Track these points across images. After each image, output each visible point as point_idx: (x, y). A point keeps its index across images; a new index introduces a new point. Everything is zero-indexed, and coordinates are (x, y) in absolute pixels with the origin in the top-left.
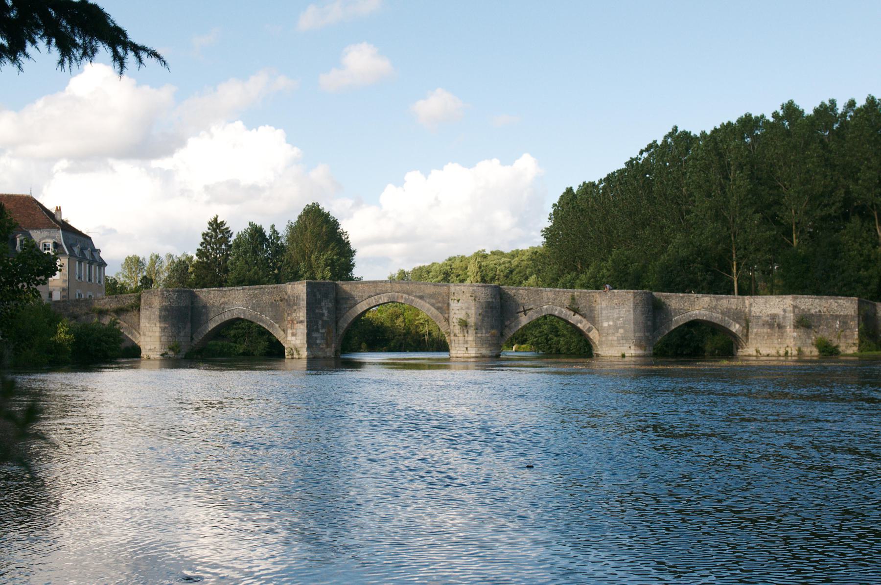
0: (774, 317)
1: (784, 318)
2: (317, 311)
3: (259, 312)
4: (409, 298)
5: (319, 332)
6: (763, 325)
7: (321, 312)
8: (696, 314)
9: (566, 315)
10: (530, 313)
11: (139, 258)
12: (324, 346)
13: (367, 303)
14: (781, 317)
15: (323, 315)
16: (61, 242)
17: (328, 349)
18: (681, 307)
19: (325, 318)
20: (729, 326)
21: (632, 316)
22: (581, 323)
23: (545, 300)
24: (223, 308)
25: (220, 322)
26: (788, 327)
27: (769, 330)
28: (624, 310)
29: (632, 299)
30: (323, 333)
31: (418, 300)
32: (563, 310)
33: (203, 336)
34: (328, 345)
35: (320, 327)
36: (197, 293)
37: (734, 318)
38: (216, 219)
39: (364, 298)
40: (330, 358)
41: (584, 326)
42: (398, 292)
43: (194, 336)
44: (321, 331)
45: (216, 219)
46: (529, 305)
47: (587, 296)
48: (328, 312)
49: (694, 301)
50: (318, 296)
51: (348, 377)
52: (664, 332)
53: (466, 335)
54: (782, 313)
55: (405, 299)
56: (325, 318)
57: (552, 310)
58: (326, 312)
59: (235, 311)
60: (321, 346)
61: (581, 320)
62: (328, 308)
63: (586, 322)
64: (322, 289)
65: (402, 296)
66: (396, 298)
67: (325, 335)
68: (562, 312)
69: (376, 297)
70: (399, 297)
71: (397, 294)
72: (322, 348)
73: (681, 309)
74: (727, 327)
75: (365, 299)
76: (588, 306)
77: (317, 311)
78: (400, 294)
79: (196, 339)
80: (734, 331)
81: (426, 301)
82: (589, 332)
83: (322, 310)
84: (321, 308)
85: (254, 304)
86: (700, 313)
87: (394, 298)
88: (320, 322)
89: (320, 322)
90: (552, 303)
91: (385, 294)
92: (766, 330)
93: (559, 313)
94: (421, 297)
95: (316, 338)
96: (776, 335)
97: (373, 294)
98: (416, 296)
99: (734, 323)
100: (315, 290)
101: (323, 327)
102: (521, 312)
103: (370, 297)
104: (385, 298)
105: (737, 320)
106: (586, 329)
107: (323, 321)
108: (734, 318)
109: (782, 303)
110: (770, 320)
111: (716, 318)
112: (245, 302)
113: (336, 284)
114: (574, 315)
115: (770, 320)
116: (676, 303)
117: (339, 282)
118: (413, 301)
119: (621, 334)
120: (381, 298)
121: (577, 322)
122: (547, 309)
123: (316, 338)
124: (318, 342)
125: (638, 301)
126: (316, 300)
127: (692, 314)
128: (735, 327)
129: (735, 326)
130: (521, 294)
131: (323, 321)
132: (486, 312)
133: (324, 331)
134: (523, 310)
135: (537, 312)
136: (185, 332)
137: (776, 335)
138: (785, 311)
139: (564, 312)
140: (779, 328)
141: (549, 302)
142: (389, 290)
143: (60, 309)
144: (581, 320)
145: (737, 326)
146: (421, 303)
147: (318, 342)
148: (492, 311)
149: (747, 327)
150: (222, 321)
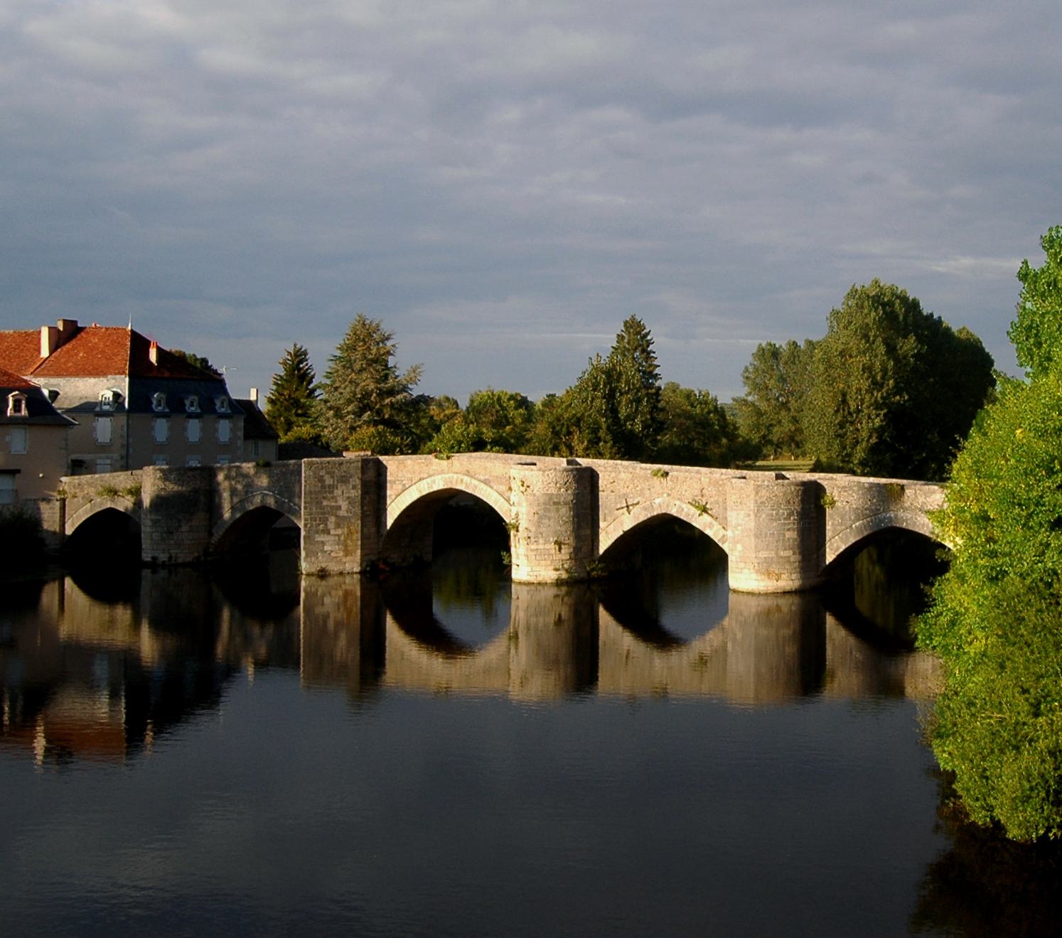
2: (325, 503)
3: (287, 498)
4: (471, 483)
5: (329, 533)
7: (333, 504)
10: (634, 510)
12: (341, 554)
13: (417, 489)
15: (339, 508)
16: (125, 393)
17: (349, 558)
19: (342, 513)
21: (753, 524)
29: (752, 496)
31: (483, 485)
32: (684, 506)
33: (224, 530)
34: (347, 553)
35: (331, 525)
36: (384, 462)
39: (414, 482)
43: (214, 531)
46: (633, 497)
47: (721, 485)
50: (328, 481)
51: (831, 657)
55: (466, 484)
56: (342, 513)
58: (344, 505)
60: (333, 554)
61: (711, 523)
65: (462, 480)
67: (342, 538)
69: (429, 480)
71: (455, 476)
72: (336, 557)
75: (415, 483)
76: (721, 500)
77: (325, 503)
78: (460, 476)
81: (492, 488)
83: (336, 502)
85: (281, 486)
87: (451, 482)
88: (332, 519)
89: (332, 519)
91: (440, 476)
94: (486, 482)
95: (323, 543)
98: (480, 481)
100: (322, 473)
101: (338, 526)
102: (623, 508)
111: (923, 525)
113: (379, 463)
117: (381, 458)
118: (476, 487)
120: (434, 482)
123: (323, 543)
125: (764, 500)
126: (323, 487)
131: (337, 517)
132: (546, 510)
133: (339, 531)
134: (625, 505)
136: (191, 526)
139: (686, 510)
142: (446, 471)
144: (711, 523)
146: (486, 490)
148: (558, 510)
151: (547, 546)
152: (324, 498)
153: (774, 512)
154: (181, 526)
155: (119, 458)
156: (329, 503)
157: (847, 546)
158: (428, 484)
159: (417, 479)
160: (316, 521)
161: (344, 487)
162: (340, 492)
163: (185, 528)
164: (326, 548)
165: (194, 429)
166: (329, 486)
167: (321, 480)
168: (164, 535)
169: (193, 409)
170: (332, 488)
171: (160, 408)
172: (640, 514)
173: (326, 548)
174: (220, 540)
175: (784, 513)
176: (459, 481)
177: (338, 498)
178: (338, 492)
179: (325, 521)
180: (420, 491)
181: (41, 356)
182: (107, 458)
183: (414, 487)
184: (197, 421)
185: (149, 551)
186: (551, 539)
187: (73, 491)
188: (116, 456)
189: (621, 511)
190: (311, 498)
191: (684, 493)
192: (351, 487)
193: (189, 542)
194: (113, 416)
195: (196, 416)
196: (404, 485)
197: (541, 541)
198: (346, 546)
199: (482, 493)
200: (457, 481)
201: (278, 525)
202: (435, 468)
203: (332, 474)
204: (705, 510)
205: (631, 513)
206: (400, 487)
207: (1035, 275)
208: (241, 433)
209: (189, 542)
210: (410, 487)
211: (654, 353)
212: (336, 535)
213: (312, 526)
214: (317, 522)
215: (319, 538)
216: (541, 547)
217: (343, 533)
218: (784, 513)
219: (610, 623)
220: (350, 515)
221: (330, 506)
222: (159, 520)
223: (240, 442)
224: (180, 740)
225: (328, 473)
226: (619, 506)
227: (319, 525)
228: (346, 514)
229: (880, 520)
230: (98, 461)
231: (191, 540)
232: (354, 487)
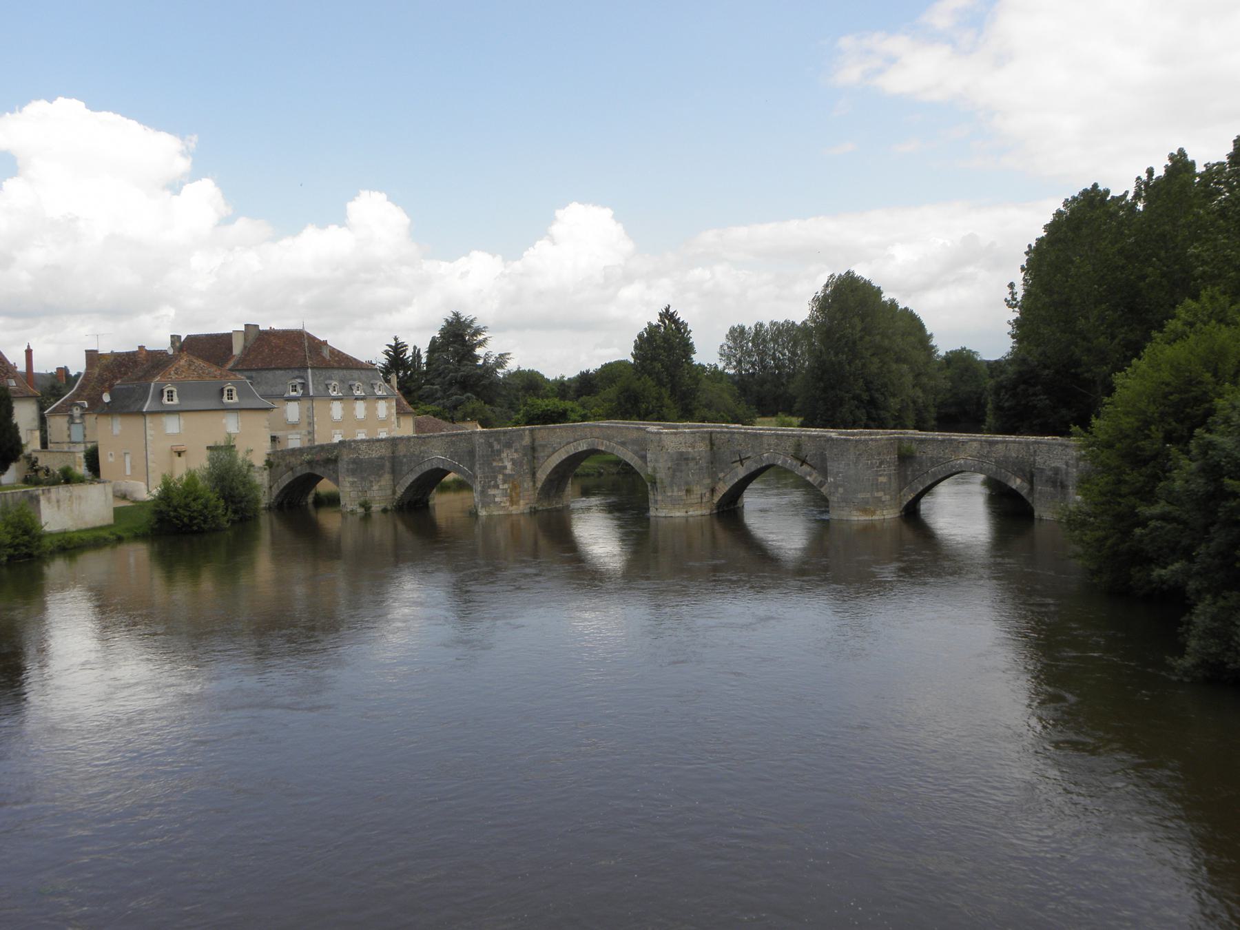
0: (1056, 471)
1: (1067, 473)
4: (610, 445)
5: (498, 488)
6: (1047, 481)
7: (500, 465)
8: (960, 464)
9: (792, 465)
10: (747, 463)
11: (744, 328)
12: (508, 504)
13: (566, 451)
14: (1064, 472)
15: (505, 468)
18: (940, 455)
20: (1007, 481)
22: (810, 476)
23: (766, 446)
24: (423, 457)
25: (420, 473)
26: (1070, 488)
27: (1052, 489)
28: (843, 462)
30: (506, 489)
35: (499, 482)
37: (1013, 470)
38: (667, 310)
39: (562, 445)
40: (774, 460)
41: (814, 481)
42: (598, 438)
44: (501, 487)
45: (667, 310)
48: (513, 464)
49: (958, 447)
50: (497, 447)
52: (917, 488)
53: (656, 493)
54: (1064, 466)
56: (508, 471)
57: (774, 459)
58: (509, 465)
59: (434, 461)
60: (502, 505)
62: (512, 459)
63: (817, 475)
64: (502, 438)
65: (602, 443)
66: (596, 444)
68: (787, 461)
69: (575, 443)
70: (600, 443)
71: (597, 440)
72: (504, 507)
73: (940, 458)
74: (1004, 481)
75: (563, 447)
79: (399, 492)
80: (1014, 487)
82: (821, 487)
83: (503, 463)
84: (501, 460)
85: (452, 452)
86: (965, 463)
88: (500, 477)
89: (500, 477)
90: (774, 450)
92: (1049, 489)
93: (782, 463)
94: (623, 444)
95: (494, 496)
96: (1059, 497)
97: (572, 440)
99: (1013, 477)
101: (505, 482)
103: (568, 443)
104: (584, 445)
105: (1016, 474)
106: (817, 483)
107: (505, 475)
108: (1013, 470)
109: (1064, 452)
110: (1053, 476)
112: (443, 450)
114: (801, 465)
115: (1053, 476)
116: (934, 449)
118: (614, 448)
119: (841, 494)
121: (807, 474)
122: (768, 458)
123: (494, 496)
124: (497, 499)
127: (956, 464)
128: (1015, 482)
129: (1015, 480)
130: (737, 439)
131: (505, 475)
133: (506, 486)
134: (738, 459)
135: (756, 462)
136: (380, 486)
137: (1059, 497)
138: (1067, 464)
140: (1062, 488)
141: (770, 449)
143: (278, 458)
145: (1018, 481)
147: (497, 499)
149: (1031, 483)
150: (423, 472)
151: (680, 494)
152: (494, 460)
153: (869, 462)
154: (372, 486)
155: (306, 433)
156: (497, 464)
157: (924, 487)
158: (574, 446)
159: (565, 443)
160: (488, 478)
161: (508, 451)
162: (505, 455)
163: (376, 487)
164: (497, 499)
165: (360, 409)
166: (497, 451)
167: (491, 446)
168: (360, 494)
169: (359, 392)
170: (499, 452)
171: (335, 393)
172: (524, 459)
173: (497, 499)
174: (402, 495)
175: (876, 463)
176: (600, 443)
177: (504, 460)
178: (504, 455)
179: (495, 478)
180: (568, 452)
181: (234, 353)
182: (297, 434)
183: (563, 449)
184: (362, 402)
185: (685, 613)
186: (683, 488)
187: (277, 461)
188: (304, 432)
189: (735, 464)
190: (484, 461)
191: (787, 448)
192: (513, 450)
193: (378, 498)
194: (299, 400)
195: (363, 398)
196: (554, 448)
197: (676, 489)
198: (511, 497)
199: (620, 452)
200: (598, 444)
201: (612, 499)
202: (579, 434)
203: (498, 441)
204: (803, 462)
205: (745, 465)
206: (551, 450)
207: (782, 324)
208: (394, 411)
209: (378, 498)
210: (559, 449)
211: (1011, 286)
212: (503, 489)
213: (485, 482)
214: (490, 479)
215: (492, 492)
216: (675, 494)
217: (509, 487)
218: (876, 463)
219: (480, 506)
220: (513, 473)
221: (499, 466)
222: (355, 482)
223: (394, 418)
224: (372, 628)
225: (496, 440)
226: (734, 460)
227: (491, 481)
228: (510, 473)
229: (952, 466)
230: (290, 437)
231: (380, 497)
232: (516, 451)
